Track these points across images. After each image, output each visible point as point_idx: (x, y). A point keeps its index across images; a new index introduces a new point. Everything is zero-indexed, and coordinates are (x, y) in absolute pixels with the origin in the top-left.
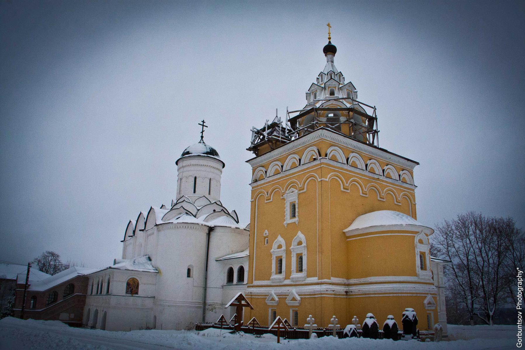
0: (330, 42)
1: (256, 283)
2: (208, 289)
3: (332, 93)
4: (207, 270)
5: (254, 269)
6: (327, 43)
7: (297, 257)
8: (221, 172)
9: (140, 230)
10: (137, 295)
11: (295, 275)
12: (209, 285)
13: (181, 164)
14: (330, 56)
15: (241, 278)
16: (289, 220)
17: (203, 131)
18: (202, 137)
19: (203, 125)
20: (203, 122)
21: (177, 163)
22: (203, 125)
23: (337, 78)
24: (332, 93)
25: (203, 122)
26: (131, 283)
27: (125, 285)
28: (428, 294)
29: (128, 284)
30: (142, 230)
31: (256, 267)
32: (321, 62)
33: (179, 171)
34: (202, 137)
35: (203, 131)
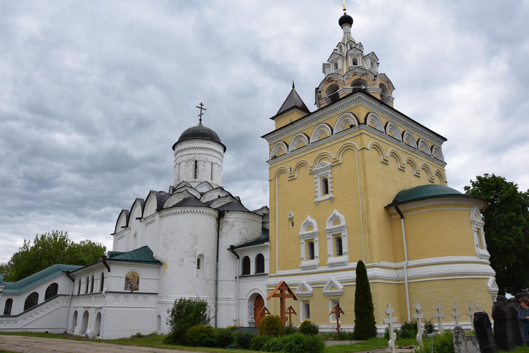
0: (345, 13)
1: (279, 273)
2: (219, 282)
3: (355, 63)
4: (217, 261)
5: (277, 258)
6: (343, 15)
7: (335, 240)
8: (223, 156)
9: (137, 219)
10: (211, 304)
11: (334, 259)
12: (219, 278)
13: (178, 148)
14: (347, 27)
15: (260, 268)
16: (321, 197)
17: (201, 114)
18: (201, 120)
19: (201, 108)
20: (201, 104)
21: (174, 148)
22: (201, 108)
23: (358, 47)
24: (355, 63)
25: (201, 104)
26: (131, 278)
27: (124, 280)
28: (489, 275)
29: (127, 279)
30: (140, 219)
31: (402, 232)
32: (339, 34)
33: (177, 156)
34: (201, 120)
35: (201, 114)
